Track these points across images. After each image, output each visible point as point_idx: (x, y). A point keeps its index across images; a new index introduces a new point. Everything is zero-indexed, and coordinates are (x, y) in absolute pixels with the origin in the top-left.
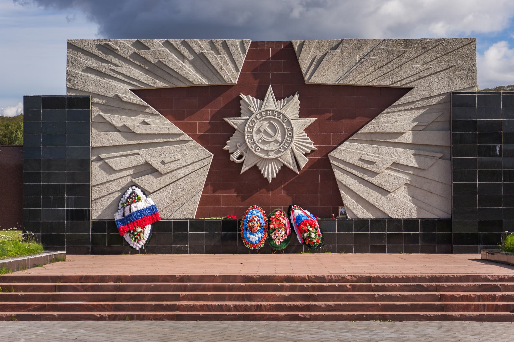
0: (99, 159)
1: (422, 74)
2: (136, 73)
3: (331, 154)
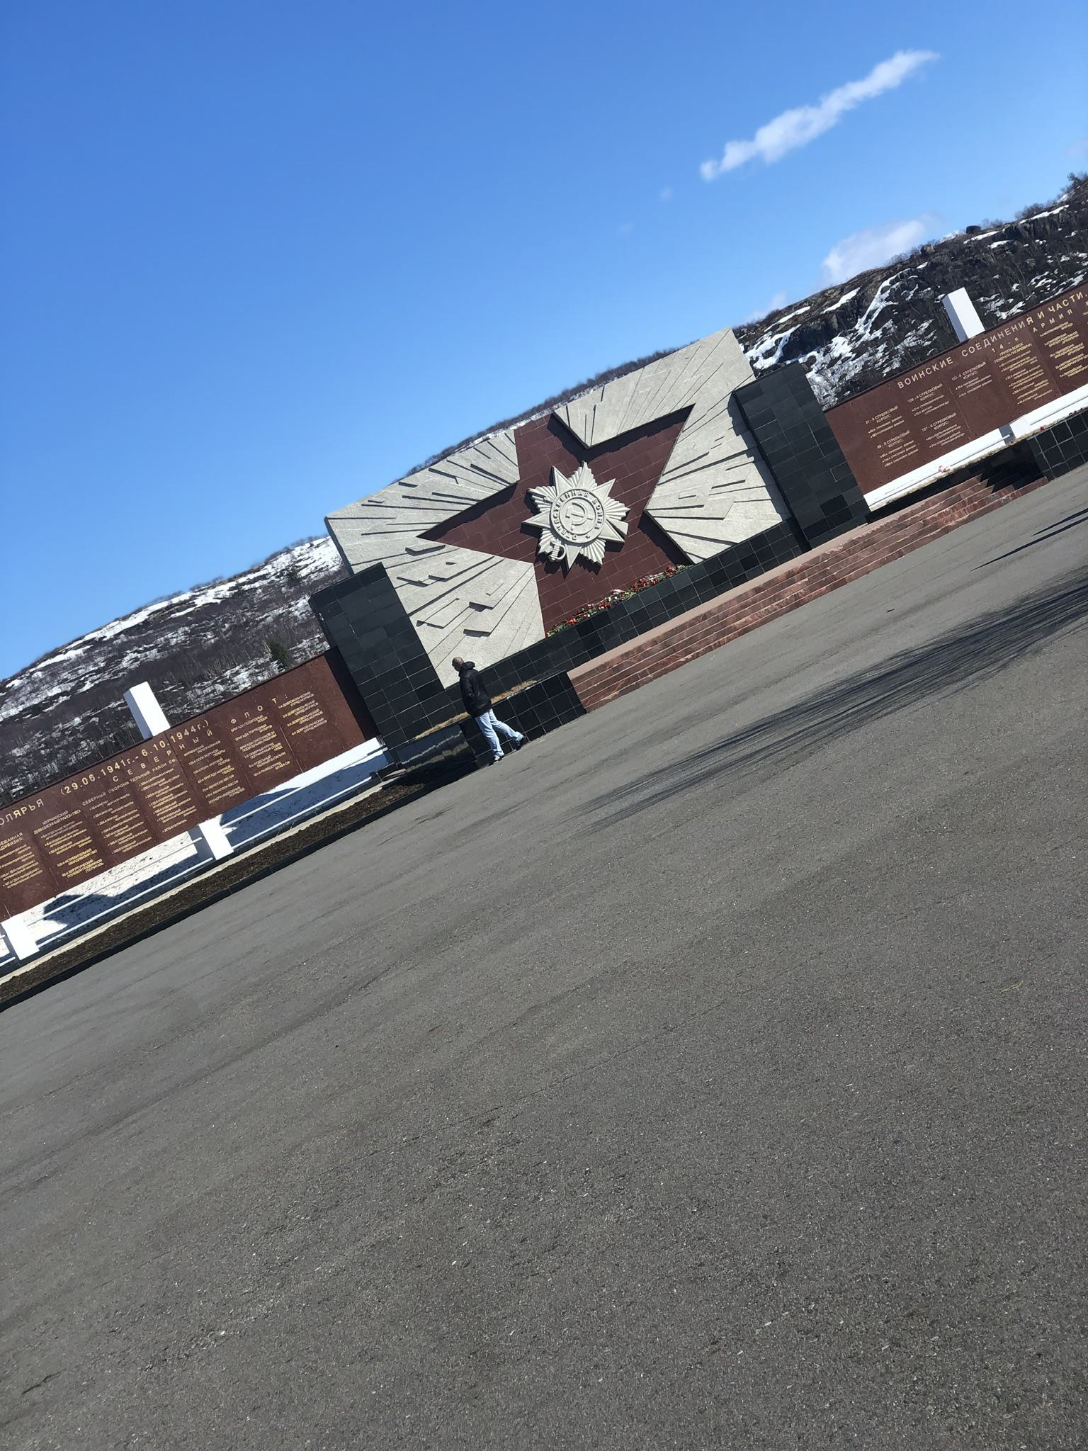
0: (420, 623)
2: (415, 516)
3: (648, 507)
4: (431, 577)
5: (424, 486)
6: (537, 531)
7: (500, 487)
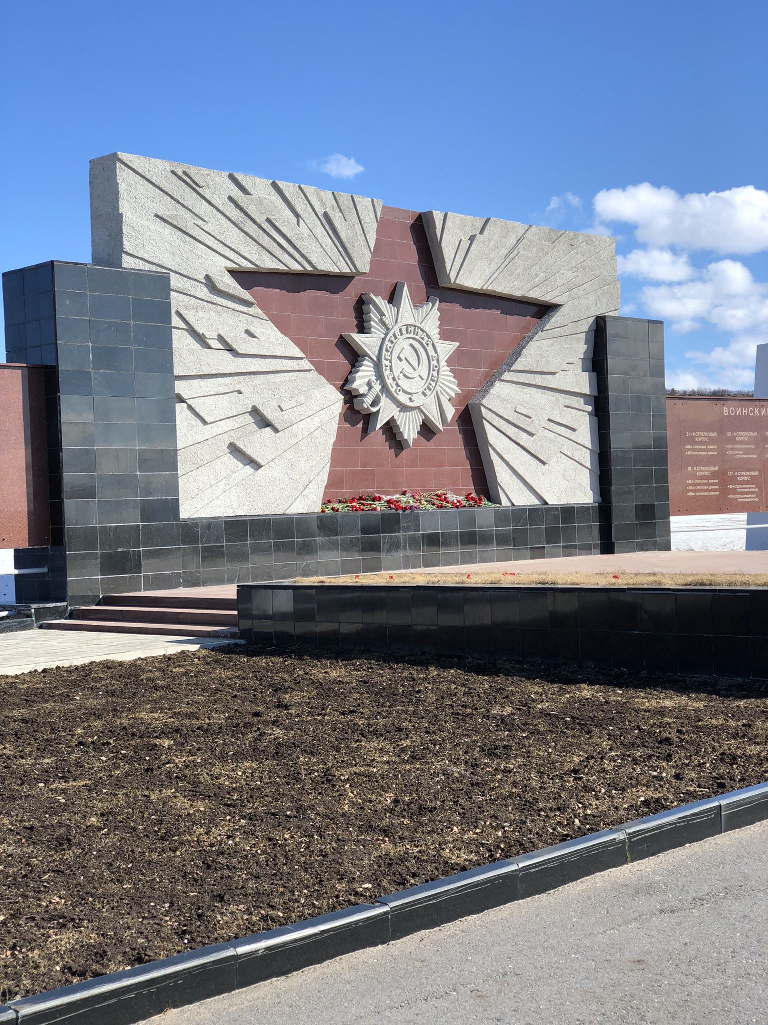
2: (234, 237)
3: (484, 402)
4: (221, 338)
5: (260, 201)
6: (354, 356)
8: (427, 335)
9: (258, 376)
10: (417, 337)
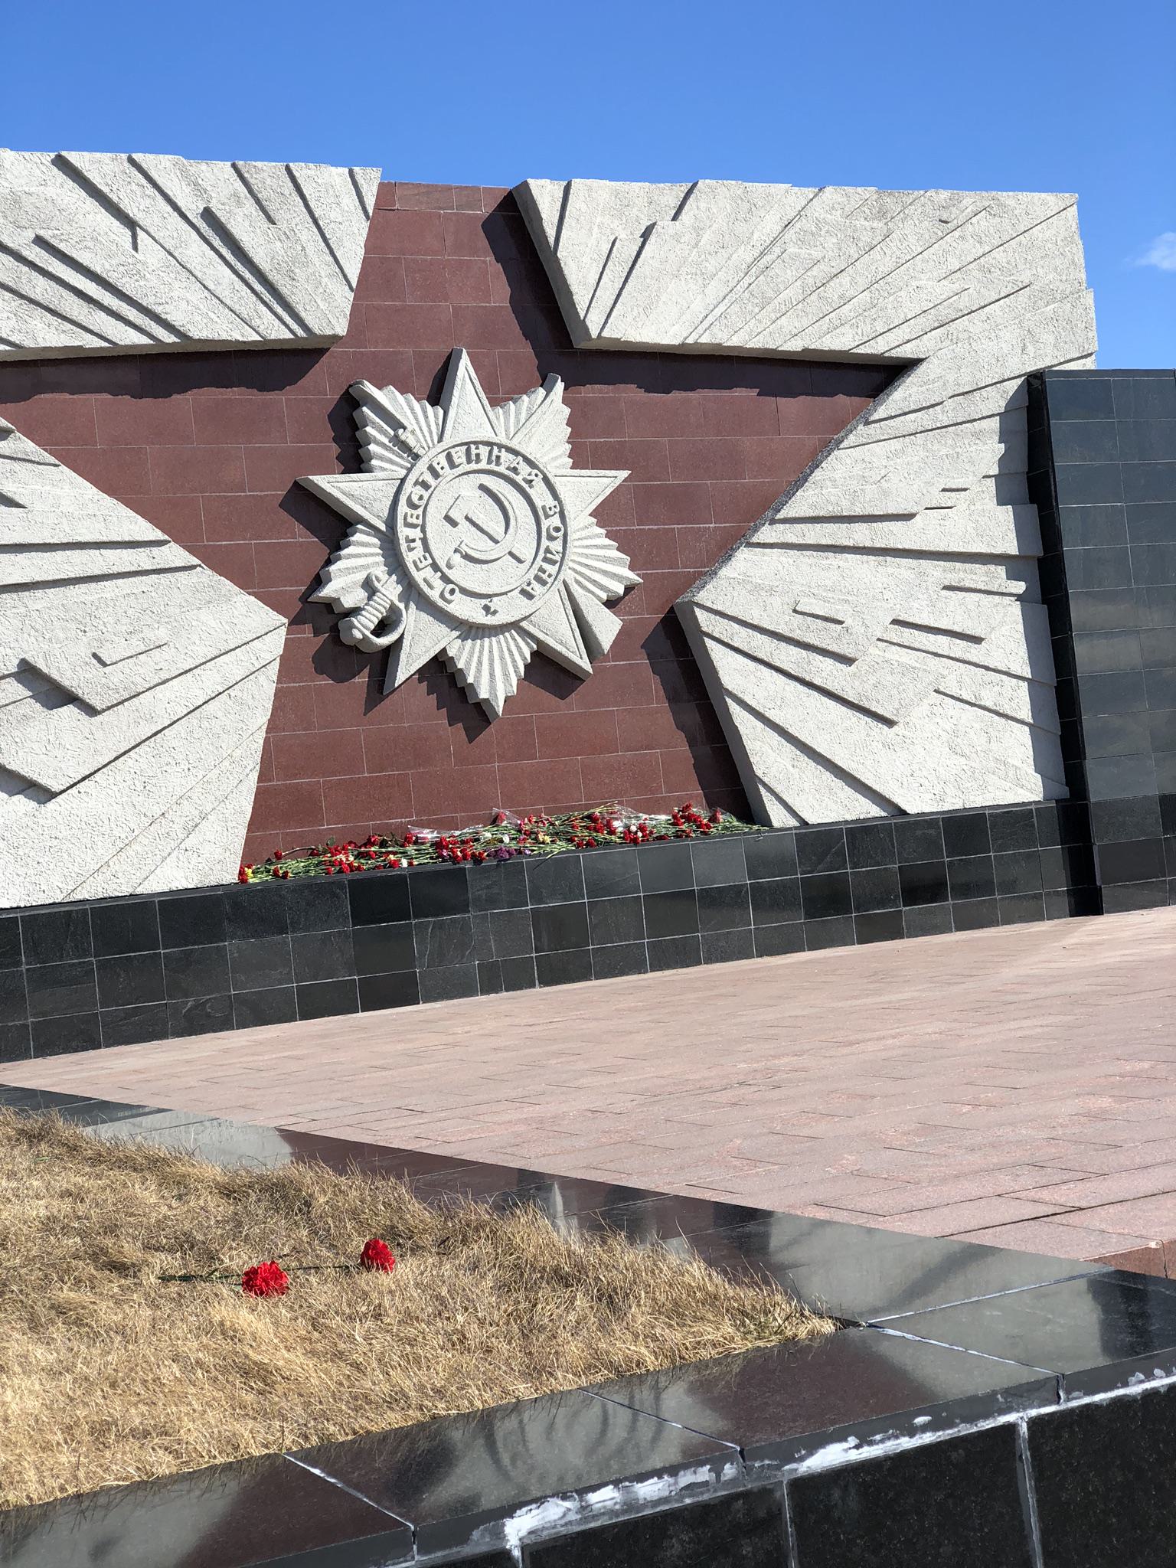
1: (946, 312)
3: (703, 597)
6: (335, 526)
7: (274, 329)
8: (527, 460)
9: (40, 593)
10: (502, 469)
